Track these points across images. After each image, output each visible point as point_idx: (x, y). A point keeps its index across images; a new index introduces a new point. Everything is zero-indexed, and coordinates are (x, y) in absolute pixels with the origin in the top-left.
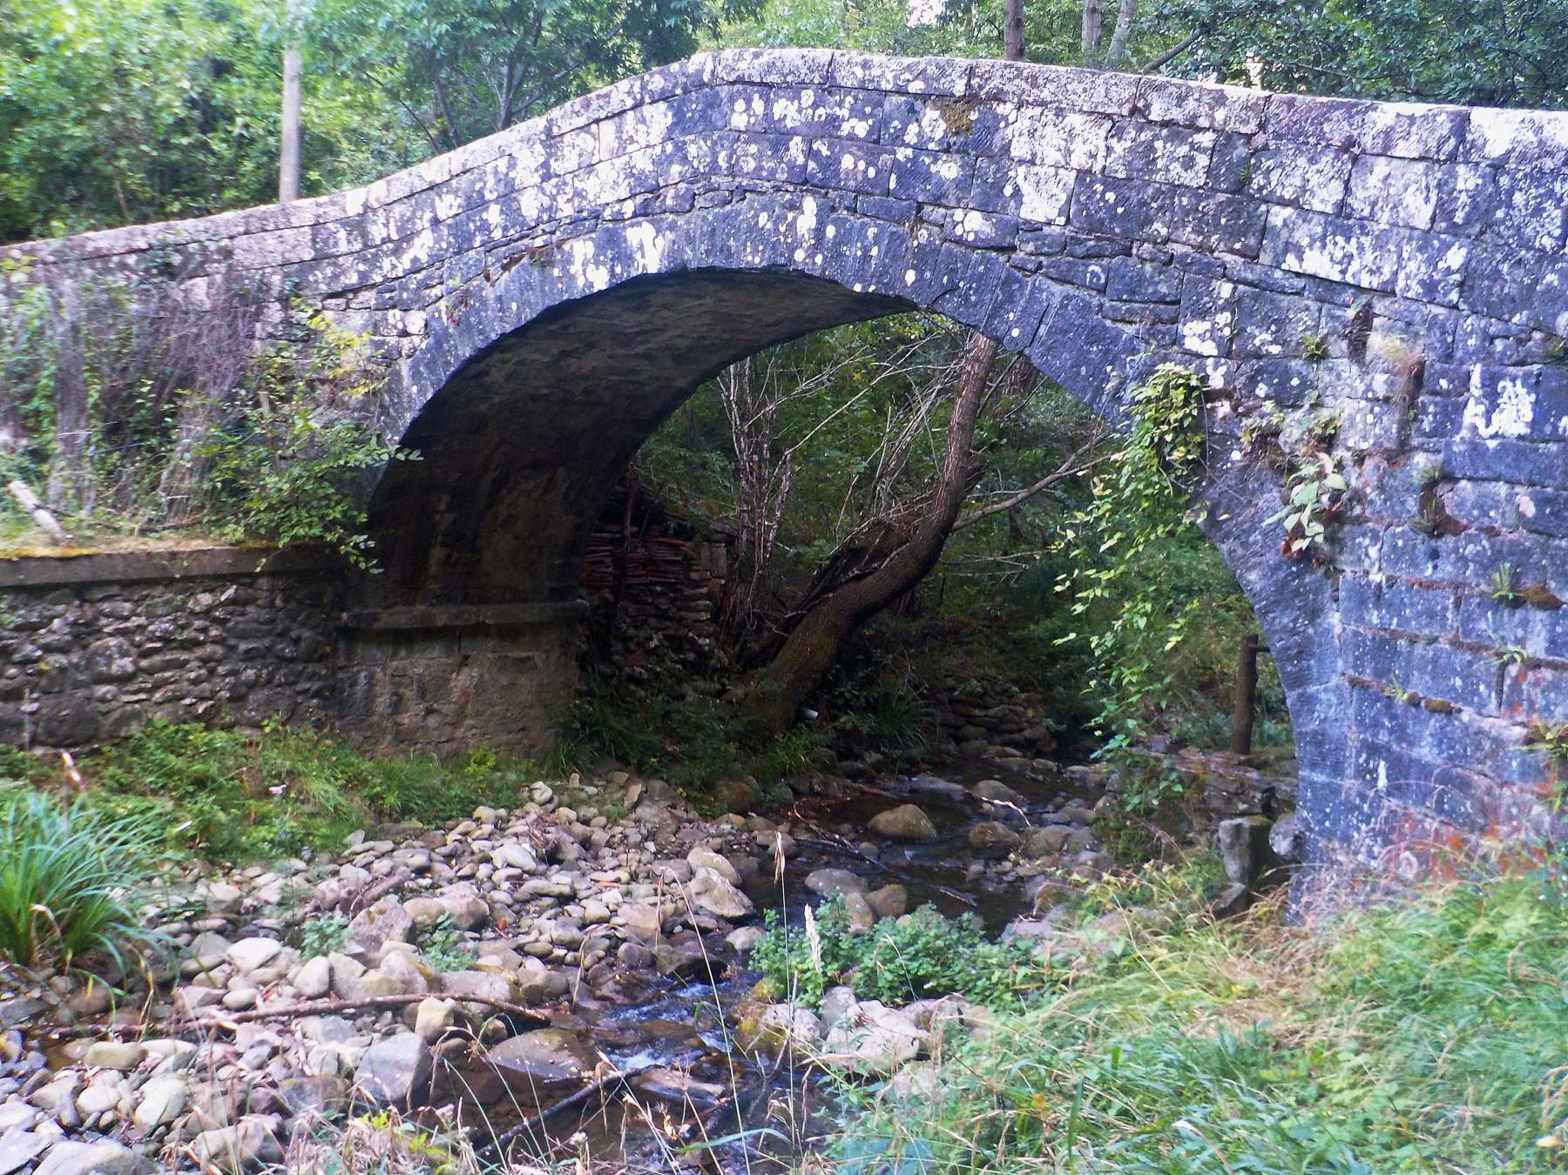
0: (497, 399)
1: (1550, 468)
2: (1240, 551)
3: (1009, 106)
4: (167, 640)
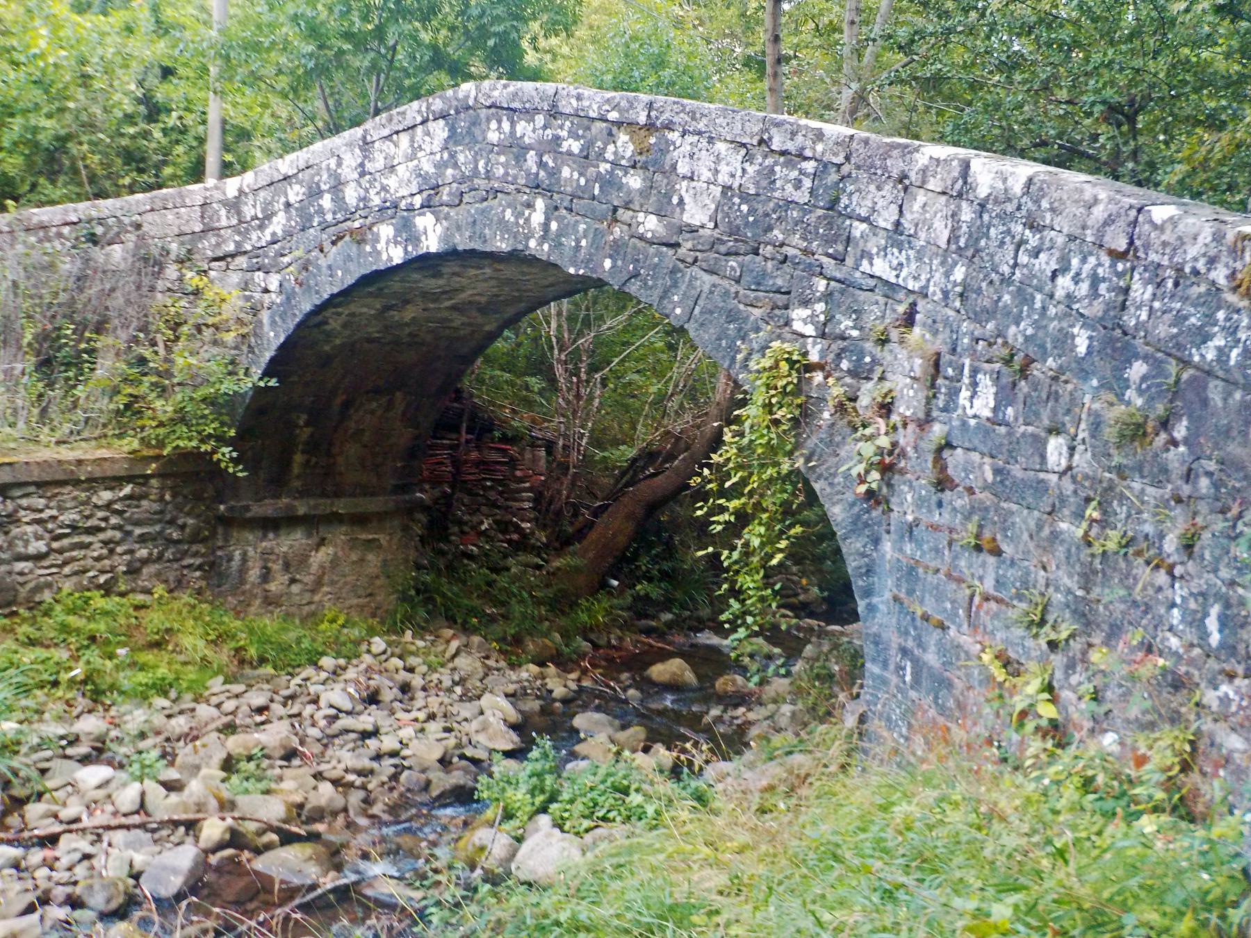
0: (338, 342)
1: (1001, 445)
2: (828, 490)
3: (677, 134)
4: (74, 527)
